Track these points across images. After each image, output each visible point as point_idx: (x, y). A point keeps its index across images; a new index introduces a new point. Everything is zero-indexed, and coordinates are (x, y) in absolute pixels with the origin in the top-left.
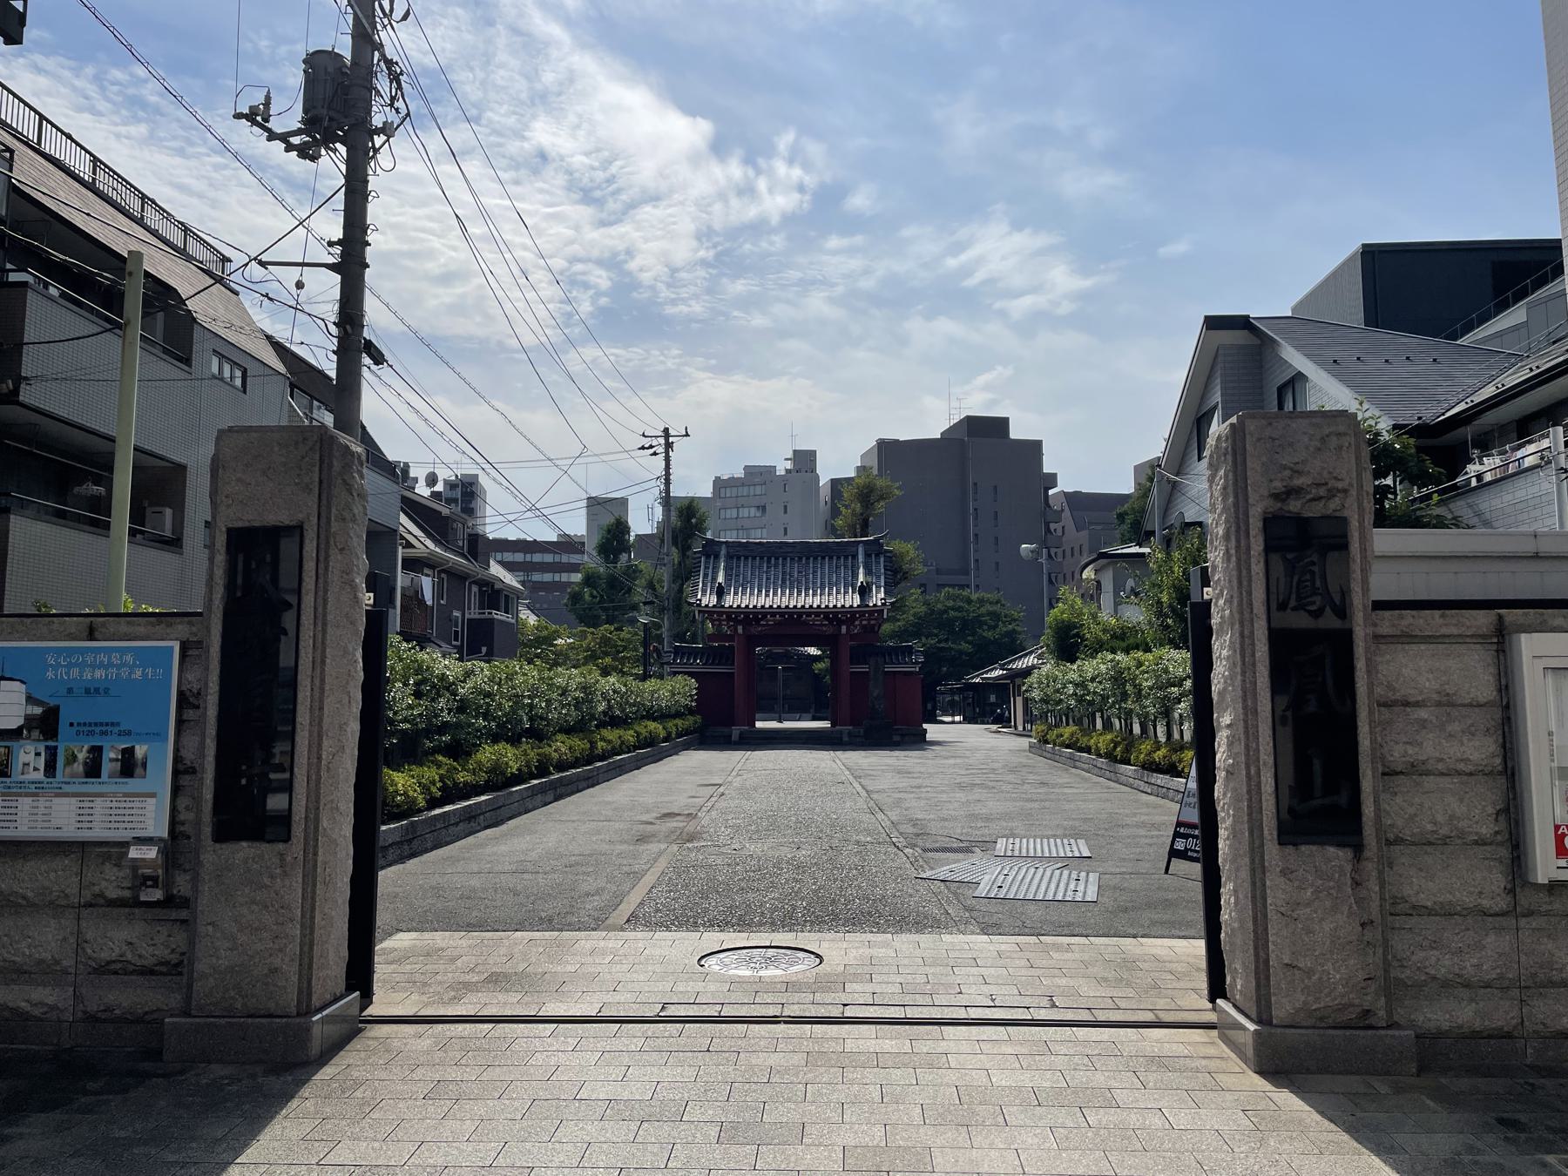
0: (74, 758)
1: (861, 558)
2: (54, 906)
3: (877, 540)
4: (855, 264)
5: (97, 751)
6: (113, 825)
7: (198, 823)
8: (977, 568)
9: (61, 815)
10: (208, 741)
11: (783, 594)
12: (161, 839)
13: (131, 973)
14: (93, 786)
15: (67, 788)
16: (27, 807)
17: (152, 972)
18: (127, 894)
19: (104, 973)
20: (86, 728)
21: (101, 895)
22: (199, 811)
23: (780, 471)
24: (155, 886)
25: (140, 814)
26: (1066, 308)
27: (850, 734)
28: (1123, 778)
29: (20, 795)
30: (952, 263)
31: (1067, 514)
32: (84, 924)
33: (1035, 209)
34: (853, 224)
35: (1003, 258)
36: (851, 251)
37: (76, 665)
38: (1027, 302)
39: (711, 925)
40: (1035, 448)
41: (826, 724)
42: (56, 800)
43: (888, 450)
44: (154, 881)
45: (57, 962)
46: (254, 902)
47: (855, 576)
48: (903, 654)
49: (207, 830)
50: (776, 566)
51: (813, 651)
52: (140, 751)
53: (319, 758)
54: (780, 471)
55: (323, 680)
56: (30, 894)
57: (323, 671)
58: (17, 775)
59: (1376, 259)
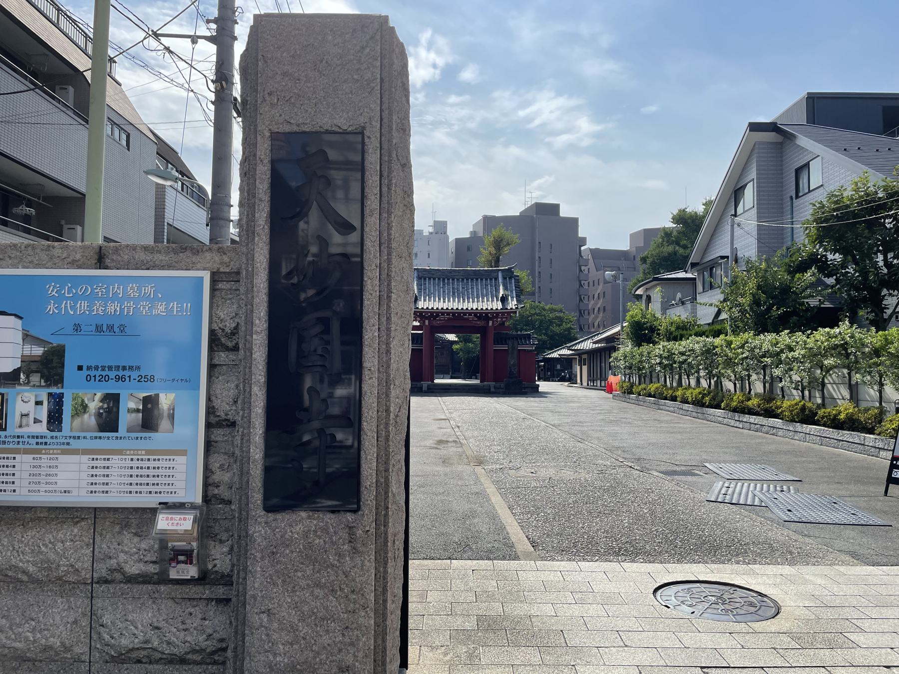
0: (85, 407)
1: (500, 280)
2: (59, 583)
3: (510, 269)
4: (465, 112)
5: (113, 400)
6: (134, 488)
7: (244, 487)
8: (540, 292)
9: (70, 477)
10: (255, 389)
11: (454, 301)
12: (193, 507)
13: (157, 662)
14: (108, 441)
15: (75, 445)
16: (26, 467)
17: (182, 661)
18: (152, 569)
19: (123, 662)
20: (94, 373)
21: (119, 570)
22: (244, 473)
23: (426, 233)
24: (189, 561)
25: (165, 474)
26: (586, 142)
27: (495, 387)
28: (710, 418)
29: (18, 451)
30: (522, 113)
31: (591, 261)
32: (98, 603)
33: (570, 84)
34: (463, 89)
35: (551, 112)
36: (462, 105)
37: (83, 297)
38: (564, 138)
39: (651, 556)
40: (573, 223)
41: (477, 382)
42: (62, 458)
43: (489, 222)
44: (188, 556)
45: (67, 649)
46: (318, 585)
47: (497, 291)
48: (525, 338)
49: (257, 497)
50: (448, 284)
51: (452, 337)
52: (165, 400)
53: (388, 411)
54: (426, 233)
55: (389, 319)
56: (31, 569)
57: (389, 307)
58: (13, 429)
59: (812, 99)
